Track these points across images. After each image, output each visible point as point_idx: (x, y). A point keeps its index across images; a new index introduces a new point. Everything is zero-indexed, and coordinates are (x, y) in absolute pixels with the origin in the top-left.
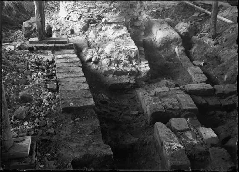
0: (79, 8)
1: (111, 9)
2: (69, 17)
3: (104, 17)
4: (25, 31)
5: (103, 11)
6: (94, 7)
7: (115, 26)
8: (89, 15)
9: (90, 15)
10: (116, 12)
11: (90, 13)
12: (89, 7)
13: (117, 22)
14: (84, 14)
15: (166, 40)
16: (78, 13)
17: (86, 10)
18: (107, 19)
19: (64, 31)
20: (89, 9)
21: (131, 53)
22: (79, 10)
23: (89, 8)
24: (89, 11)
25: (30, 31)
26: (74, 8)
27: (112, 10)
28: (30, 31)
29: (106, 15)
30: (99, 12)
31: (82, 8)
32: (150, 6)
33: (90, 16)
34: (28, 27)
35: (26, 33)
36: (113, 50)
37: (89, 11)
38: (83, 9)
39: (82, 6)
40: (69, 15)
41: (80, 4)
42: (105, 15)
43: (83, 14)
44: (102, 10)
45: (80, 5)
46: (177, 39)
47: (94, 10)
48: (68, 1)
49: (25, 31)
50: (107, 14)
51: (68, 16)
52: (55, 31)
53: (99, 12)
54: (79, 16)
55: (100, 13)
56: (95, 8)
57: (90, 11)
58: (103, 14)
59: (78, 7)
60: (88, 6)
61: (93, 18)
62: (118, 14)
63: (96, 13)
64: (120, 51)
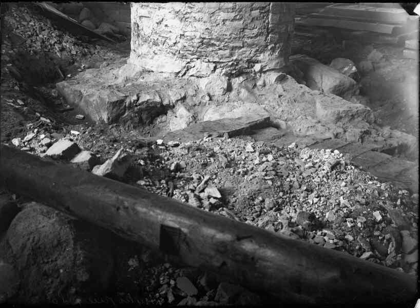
0: (212, 51)
1: (267, 46)
2: (188, 70)
3: (257, 62)
4: (113, 109)
5: (256, 51)
6: (242, 46)
7: (279, 76)
8: (232, 60)
9: (235, 60)
10: (273, 50)
11: (234, 58)
12: (233, 47)
13: (278, 67)
14: (225, 61)
15: (339, 90)
16: (211, 61)
17: (227, 52)
18: (264, 64)
19: (194, 98)
20: (232, 50)
21: (369, 115)
22: (213, 53)
23: (233, 48)
24: (231, 55)
25: (121, 108)
26: (200, 52)
27: (269, 47)
28: (121, 108)
29: (261, 57)
30: (250, 53)
31: (220, 49)
32: (221, 49)
33: (235, 63)
34: (117, 101)
35: (114, 115)
36: (341, 115)
37: (231, 55)
38: (220, 52)
39: (219, 45)
40: (188, 67)
41: (215, 43)
42: (260, 58)
43: (221, 61)
44: (254, 50)
45: (215, 45)
46: (353, 85)
47: (241, 50)
48: (397, 4)
49: (113, 109)
50: (262, 55)
51: (185, 69)
52: (179, 100)
53: (250, 53)
54: (212, 66)
55: (251, 55)
56: (243, 47)
57: (235, 53)
58: (257, 56)
59: (211, 49)
60: (231, 45)
61: (240, 66)
62: (277, 53)
63: (244, 56)
64: (352, 115)
